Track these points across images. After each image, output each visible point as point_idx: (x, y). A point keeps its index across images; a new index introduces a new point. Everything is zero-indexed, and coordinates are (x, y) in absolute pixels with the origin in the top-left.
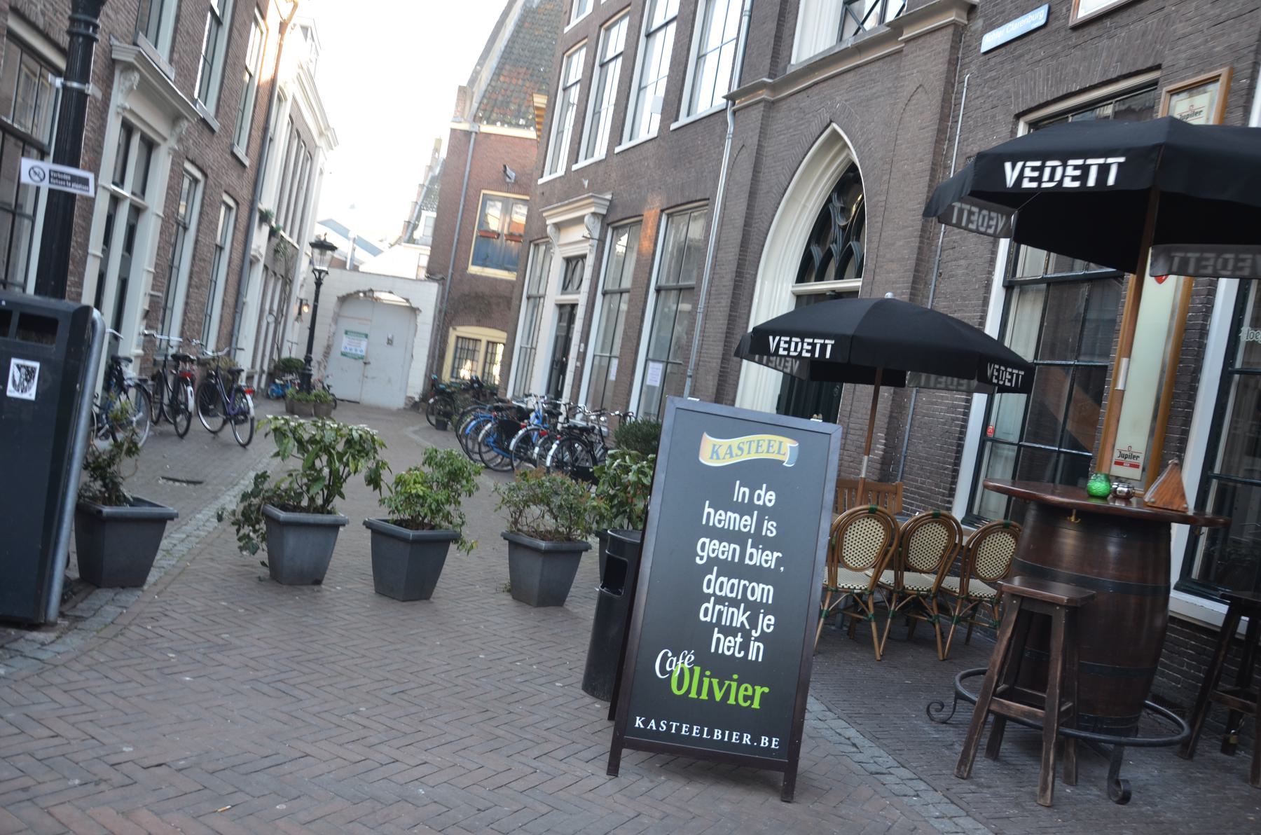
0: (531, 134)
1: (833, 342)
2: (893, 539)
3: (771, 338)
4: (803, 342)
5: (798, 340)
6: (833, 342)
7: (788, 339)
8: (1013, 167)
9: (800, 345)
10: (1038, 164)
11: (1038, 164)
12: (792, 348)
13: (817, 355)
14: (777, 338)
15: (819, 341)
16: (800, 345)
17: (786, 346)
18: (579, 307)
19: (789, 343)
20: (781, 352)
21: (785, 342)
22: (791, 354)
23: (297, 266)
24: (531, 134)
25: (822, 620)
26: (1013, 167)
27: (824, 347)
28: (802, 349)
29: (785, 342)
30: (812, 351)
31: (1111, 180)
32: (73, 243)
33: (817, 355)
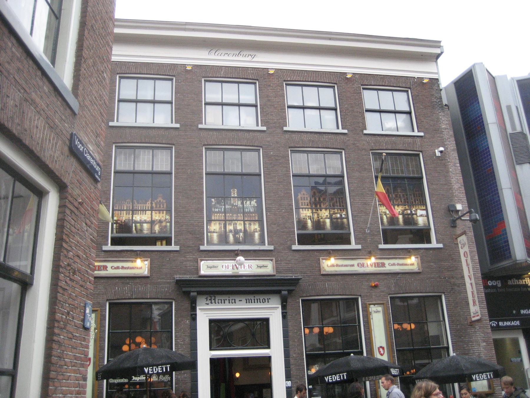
0: (110, 359)
1: (169, 365)
2: (229, 371)
3: (325, 378)
4: (336, 376)
5: (334, 376)
6: (169, 365)
7: (331, 376)
8: (326, 378)
9: (335, 377)
10: (152, 367)
11: (152, 367)
12: (333, 379)
13: (342, 379)
14: (327, 377)
15: (341, 374)
16: (335, 377)
17: (331, 378)
18: (208, 264)
19: (332, 377)
20: (150, 372)
21: (330, 378)
22: (155, 372)
23: (5, 17)
24: (110, 359)
25: (69, 360)
26: (326, 378)
27: (343, 376)
28: (336, 378)
29: (330, 378)
30: (340, 378)
31: (345, 378)
32: (458, 165)
33: (342, 379)
